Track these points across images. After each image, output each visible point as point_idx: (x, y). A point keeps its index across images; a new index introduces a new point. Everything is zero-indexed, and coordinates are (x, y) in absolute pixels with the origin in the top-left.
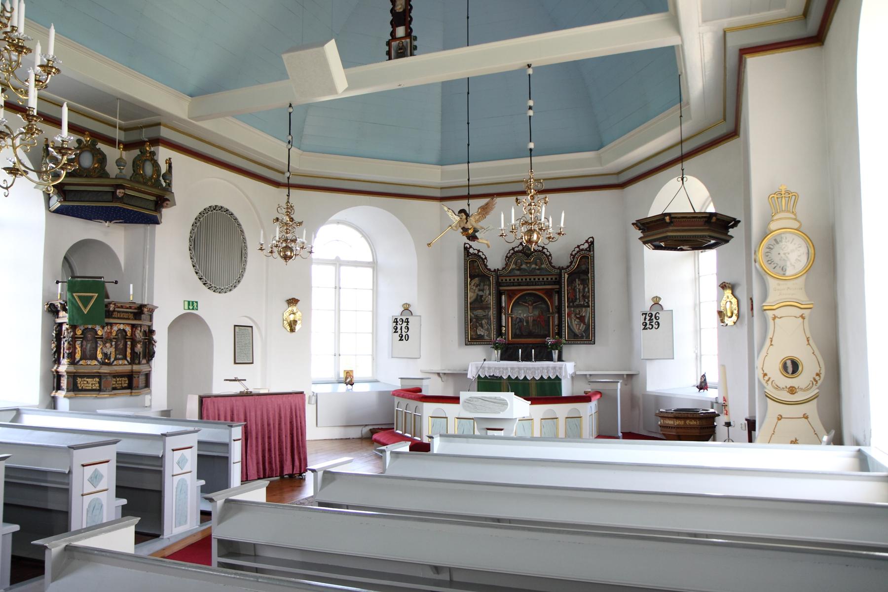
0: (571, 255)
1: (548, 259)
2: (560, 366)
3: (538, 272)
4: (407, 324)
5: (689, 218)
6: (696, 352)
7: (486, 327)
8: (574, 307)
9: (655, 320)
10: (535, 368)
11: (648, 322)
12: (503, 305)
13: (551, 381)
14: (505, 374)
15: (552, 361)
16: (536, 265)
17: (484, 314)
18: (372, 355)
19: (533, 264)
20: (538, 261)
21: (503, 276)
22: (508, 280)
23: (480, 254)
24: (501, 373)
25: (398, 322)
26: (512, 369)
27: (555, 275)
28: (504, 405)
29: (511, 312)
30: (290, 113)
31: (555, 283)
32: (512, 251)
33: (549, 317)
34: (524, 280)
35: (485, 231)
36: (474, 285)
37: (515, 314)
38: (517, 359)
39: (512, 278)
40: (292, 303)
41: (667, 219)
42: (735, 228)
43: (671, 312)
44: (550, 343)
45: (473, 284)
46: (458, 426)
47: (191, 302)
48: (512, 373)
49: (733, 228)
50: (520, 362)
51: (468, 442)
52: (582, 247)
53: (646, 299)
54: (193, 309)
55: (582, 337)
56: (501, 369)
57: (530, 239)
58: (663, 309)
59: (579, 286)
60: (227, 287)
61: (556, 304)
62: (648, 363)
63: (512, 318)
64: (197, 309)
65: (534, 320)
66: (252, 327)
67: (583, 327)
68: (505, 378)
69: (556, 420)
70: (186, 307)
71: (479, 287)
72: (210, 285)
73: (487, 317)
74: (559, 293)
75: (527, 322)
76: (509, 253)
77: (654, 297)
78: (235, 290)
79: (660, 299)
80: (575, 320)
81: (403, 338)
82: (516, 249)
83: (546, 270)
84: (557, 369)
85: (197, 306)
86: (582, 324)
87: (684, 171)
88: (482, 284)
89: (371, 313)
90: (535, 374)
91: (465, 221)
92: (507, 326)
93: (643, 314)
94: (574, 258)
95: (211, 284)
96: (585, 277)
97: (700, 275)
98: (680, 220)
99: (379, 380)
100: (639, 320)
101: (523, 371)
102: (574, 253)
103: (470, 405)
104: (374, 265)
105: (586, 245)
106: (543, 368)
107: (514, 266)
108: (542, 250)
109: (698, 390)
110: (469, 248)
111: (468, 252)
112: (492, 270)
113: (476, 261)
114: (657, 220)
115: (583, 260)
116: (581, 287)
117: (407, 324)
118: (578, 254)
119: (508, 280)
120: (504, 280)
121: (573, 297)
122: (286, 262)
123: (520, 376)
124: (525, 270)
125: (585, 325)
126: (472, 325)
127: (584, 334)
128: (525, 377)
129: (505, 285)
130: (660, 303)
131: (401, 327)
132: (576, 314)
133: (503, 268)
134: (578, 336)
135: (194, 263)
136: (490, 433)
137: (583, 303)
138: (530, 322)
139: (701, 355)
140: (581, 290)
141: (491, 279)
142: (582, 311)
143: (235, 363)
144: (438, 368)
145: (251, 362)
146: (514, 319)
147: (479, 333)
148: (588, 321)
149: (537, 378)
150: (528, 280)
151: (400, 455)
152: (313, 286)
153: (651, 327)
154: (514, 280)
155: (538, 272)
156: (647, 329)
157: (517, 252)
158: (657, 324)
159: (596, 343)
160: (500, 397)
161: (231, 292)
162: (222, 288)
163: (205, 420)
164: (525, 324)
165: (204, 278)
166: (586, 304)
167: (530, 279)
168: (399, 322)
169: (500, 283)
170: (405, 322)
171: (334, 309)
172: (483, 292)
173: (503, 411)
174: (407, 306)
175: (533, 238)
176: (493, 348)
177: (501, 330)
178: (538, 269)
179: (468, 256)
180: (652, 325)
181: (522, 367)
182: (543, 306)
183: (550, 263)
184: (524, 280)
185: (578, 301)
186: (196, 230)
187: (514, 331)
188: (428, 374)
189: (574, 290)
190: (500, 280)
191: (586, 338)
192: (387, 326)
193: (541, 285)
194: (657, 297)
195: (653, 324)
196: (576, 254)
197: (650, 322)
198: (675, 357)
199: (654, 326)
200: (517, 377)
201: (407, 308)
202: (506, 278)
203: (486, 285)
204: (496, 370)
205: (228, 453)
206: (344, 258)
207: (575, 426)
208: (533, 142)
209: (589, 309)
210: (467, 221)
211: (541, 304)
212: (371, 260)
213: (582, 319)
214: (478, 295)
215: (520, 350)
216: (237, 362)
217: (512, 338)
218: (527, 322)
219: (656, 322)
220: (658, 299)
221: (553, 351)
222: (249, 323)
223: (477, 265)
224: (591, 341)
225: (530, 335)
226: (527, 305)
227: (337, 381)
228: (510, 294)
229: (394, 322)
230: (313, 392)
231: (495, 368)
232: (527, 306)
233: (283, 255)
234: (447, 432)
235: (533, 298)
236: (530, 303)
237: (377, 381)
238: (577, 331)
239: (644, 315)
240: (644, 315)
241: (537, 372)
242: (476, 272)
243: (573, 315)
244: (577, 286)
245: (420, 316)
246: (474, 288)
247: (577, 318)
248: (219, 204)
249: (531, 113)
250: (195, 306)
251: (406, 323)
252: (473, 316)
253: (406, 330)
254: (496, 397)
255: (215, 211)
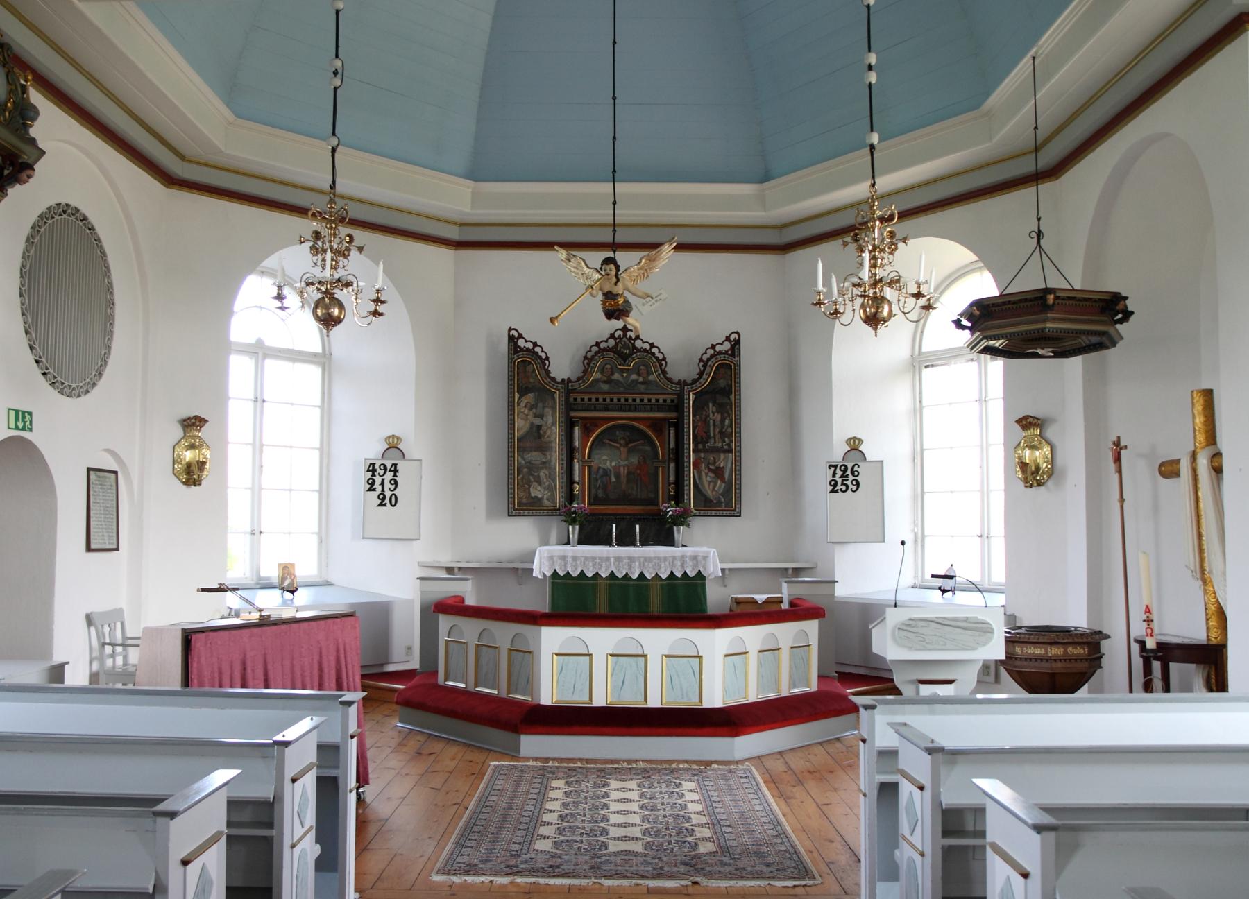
0: (701, 360)
1: (661, 365)
2: (705, 555)
3: (642, 388)
4: (395, 476)
5: (1014, 303)
6: (916, 531)
7: (547, 484)
8: (705, 451)
9: (851, 478)
10: (659, 558)
11: (839, 481)
12: (577, 444)
13: (617, 582)
14: (603, 569)
15: (673, 546)
16: (639, 375)
17: (544, 460)
18: (319, 534)
19: (633, 373)
20: (642, 367)
21: (578, 393)
22: (586, 399)
23: (538, 349)
24: (597, 567)
25: (376, 470)
26: (618, 559)
27: (671, 394)
28: (985, 632)
29: (589, 457)
30: (337, 12)
31: (669, 409)
32: (595, 349)
33: (657, 468)
34: (615, 400)
35: (653, 301)
36: (525, 407)
37: (596, 461)
38: (608, 542)
39: (594, 396)
40: (194, 424)
41: (1051, 297)
42: (1125, 324)
43: (880, 463)
44: (670, 513)
45: (523, 404)
46: (612, 675)
47: (20, 413)
48: (618, 567)
49: (1122, 323)
50: (614, 546)
51: (932, 713)
52: (718, 348)
53: (834, 442)
54: (23, 429)
55: (719, 503)
56: (598, 561)
57: (876, 314)
58: (865, 459)
59: (714, 415)
60: (81, 384)
61: (672, 445)
62: (837, 548)
63: (590, 468)
64: (31, 430)
65: (629, 473)
66: (116, 473)
67: (720, 486)
68: (604, 575)
69: (777, 652)
70: (12, 425)
71: (534, 410)
72: (55, 377)
73: (545, 464)
74: (678, 426)
75: (618, 476)
76: (590, 351)
77: (851, 439)
78: (95, 392)
79: (860, 441)
80: (707, 475)
81: (387, 501)
82: (602, 345)
83: (657, 385)
84: (700, 559)
85: (31, 424)
86: (719, 482)
87: (1041, 221)
88: (540, 405)
89: (317, 453)
90: (660, 569)
91: (614, 280)
92: (582, 483)
93: (830, 467)
94: (705, 366)
95: (56, 375)
96: (726, 400)
97: (924, 403)
98: (1064, 302)
99: (331, 580)
100: (816, 479)
101: (637, 563)
102: (705, 358)
103: (909, 635)
104: (324, 359)
105: (727, 346)
106: (674, 558)
107: (598, 376)
108: (650, 349)
109: (941, 593)
110: (518, 339)
111: (516, 345)
112: (559, 380)
113: (530, 363)
114: (1020, 301)
115: (722, 370)
116: (718, 417)
117: (395, 476)
118: (713, 359)
119: (586, 399)
120: (579, 400)
121: (704, 435)
122: (328, 329)
123: (634, 573)
124: (617, 383)
125: (725, 483)
126: (522, 479)
127: (723, 499)
128: (642, 574)
129: (580, 408)
130: (860, 449)
131: (383, 480)
132: (709, 464)
133: (579, 379)
134: (712, 501)
135: (27, 326)
136: (926, 690)
137: (720, 445)
138: (622, 475)
139: (923, 536)
140: (718, 423)
141: (557, 396)
142: (719, 459)
143: (89, 549)
144: (446, 559)
145: (115, 547)
146: (594, 470)
147: (533, 495)
148: (729, 476)
149: (664, 576)
150: (623, 400)
151: (959, 757)
152: (231, 394)
153: (844, 488)
154: (597, 400)
155: (642, 388)
156: (837, 491)
157: (605, 350)
158: (854, 483)
159: (742, 515)
160: (977, 617)
161: (88, 395)
162: (74, 385)
163: (194, 689)
164: (613, 479)
165: (44, 360)
166: (726, 447)
167: (642, 400)
168: (378, 471)
169: (571, 404)
170: (390, 471)
171: (251, 441)
172: (542, 419)
173: (984, 644)
174: (396, 441)
175: (882, 312)
176: (565, 521)
177: (571, 490)
178: (642, 383)
179: (516, 352)
180: (847, 486)
181: (636, 556)
182: (648, 448)
183: (664, 372)
184: (615, 400)
185: (712, 441)
186: (32, 251)
187: (593, 491)
188: (430, 570)
189: (705, 421)
190: (571, 400)
191: (725, 507)
192: (351, 480)
193: (645, 411)
194: (855, 438)
195: (848, 483)
196: (708, 360)
197: (843, 480)
198: (886, 539)
199: (851, 487)
200: (627, 574)
201: (393, 445)
202: (583, 396)
203: (547, 407)
204: (587, 563)
205: (337, 767)
206: (271, 342)
207: (801, 661)
208: (877, 132)
209: (731, 456)
210: (618, 280)
211: (642, 445)
212: (319, 350)
213: (718, 473)
214: (532, 424)
215: (638, 527)
216: (93, 546)
217: (590, 504)
218: (618, 476)
219: (854, 480)
220: (857, 442)
221: (675, 528)
222: (110, 464)
223: (531, 370)
224: (735, 510)
225: (625, 499)
226: (618, 445)
227: (257, 584)
228: (589, 425)
229: (368, 471)
230: (231, 609)
231: (586, 558)
232: (617, 447)
233: (323, 314)
234: (701, 701)
235: (628, 434)
236: (622, 442)
237: (328, 584)
238: (709, 493)
239: (833, 469)
240: (833, 469)
241: (663, 565)
242: (530, 382)
243: (703, 465)
244: (711, 415)
245: (420, 460)
246: (526, 411)
247: (710, 470)
248: (74, 203)
249: (873, 77)
250: (28, 423)
251: (392, 474)
252: (523, 462)
253: (392, 487)
254: (967, 618)
255: (65, 216)
